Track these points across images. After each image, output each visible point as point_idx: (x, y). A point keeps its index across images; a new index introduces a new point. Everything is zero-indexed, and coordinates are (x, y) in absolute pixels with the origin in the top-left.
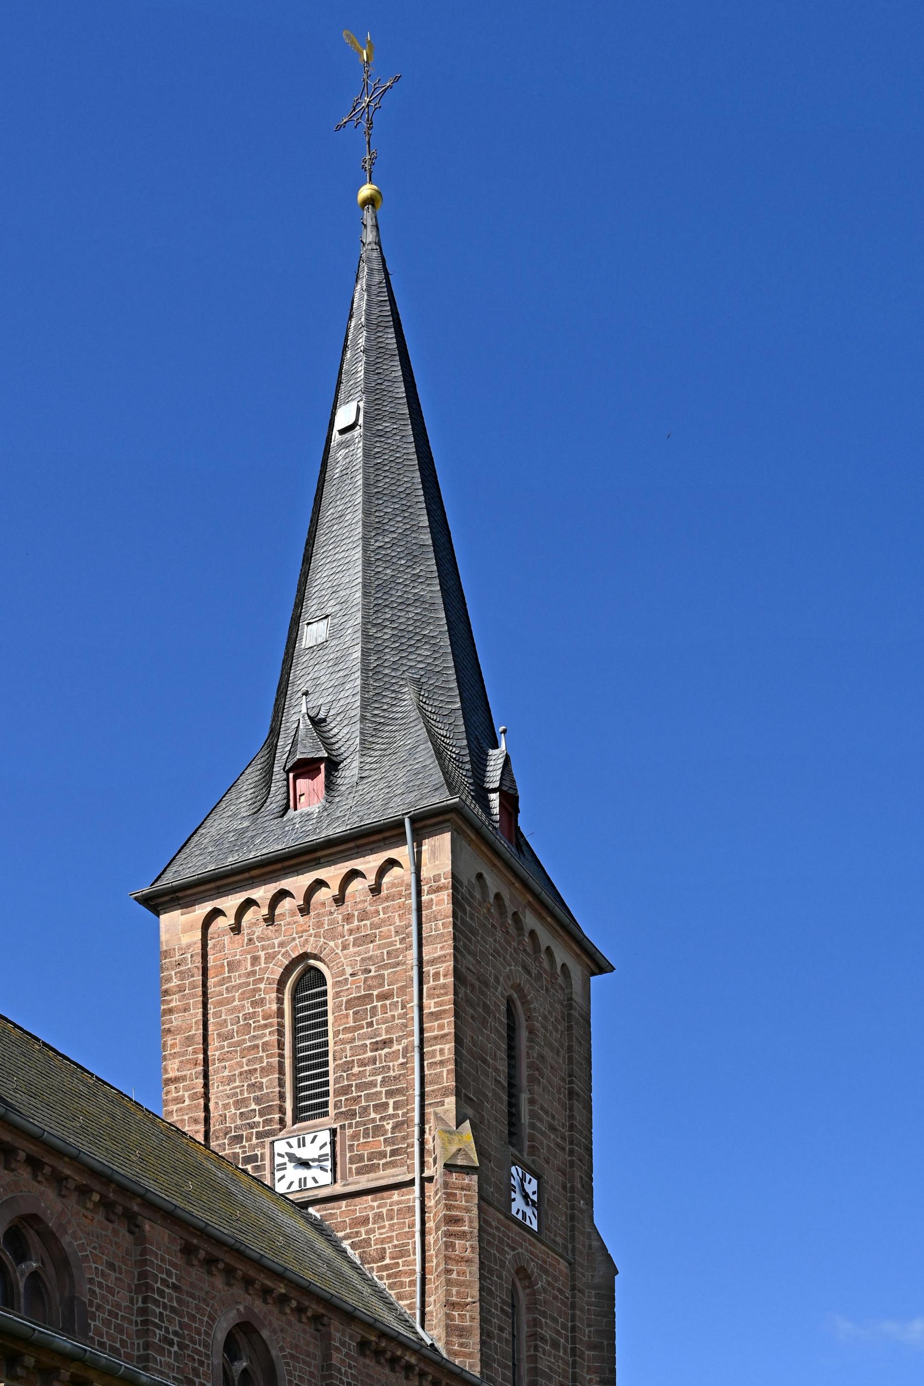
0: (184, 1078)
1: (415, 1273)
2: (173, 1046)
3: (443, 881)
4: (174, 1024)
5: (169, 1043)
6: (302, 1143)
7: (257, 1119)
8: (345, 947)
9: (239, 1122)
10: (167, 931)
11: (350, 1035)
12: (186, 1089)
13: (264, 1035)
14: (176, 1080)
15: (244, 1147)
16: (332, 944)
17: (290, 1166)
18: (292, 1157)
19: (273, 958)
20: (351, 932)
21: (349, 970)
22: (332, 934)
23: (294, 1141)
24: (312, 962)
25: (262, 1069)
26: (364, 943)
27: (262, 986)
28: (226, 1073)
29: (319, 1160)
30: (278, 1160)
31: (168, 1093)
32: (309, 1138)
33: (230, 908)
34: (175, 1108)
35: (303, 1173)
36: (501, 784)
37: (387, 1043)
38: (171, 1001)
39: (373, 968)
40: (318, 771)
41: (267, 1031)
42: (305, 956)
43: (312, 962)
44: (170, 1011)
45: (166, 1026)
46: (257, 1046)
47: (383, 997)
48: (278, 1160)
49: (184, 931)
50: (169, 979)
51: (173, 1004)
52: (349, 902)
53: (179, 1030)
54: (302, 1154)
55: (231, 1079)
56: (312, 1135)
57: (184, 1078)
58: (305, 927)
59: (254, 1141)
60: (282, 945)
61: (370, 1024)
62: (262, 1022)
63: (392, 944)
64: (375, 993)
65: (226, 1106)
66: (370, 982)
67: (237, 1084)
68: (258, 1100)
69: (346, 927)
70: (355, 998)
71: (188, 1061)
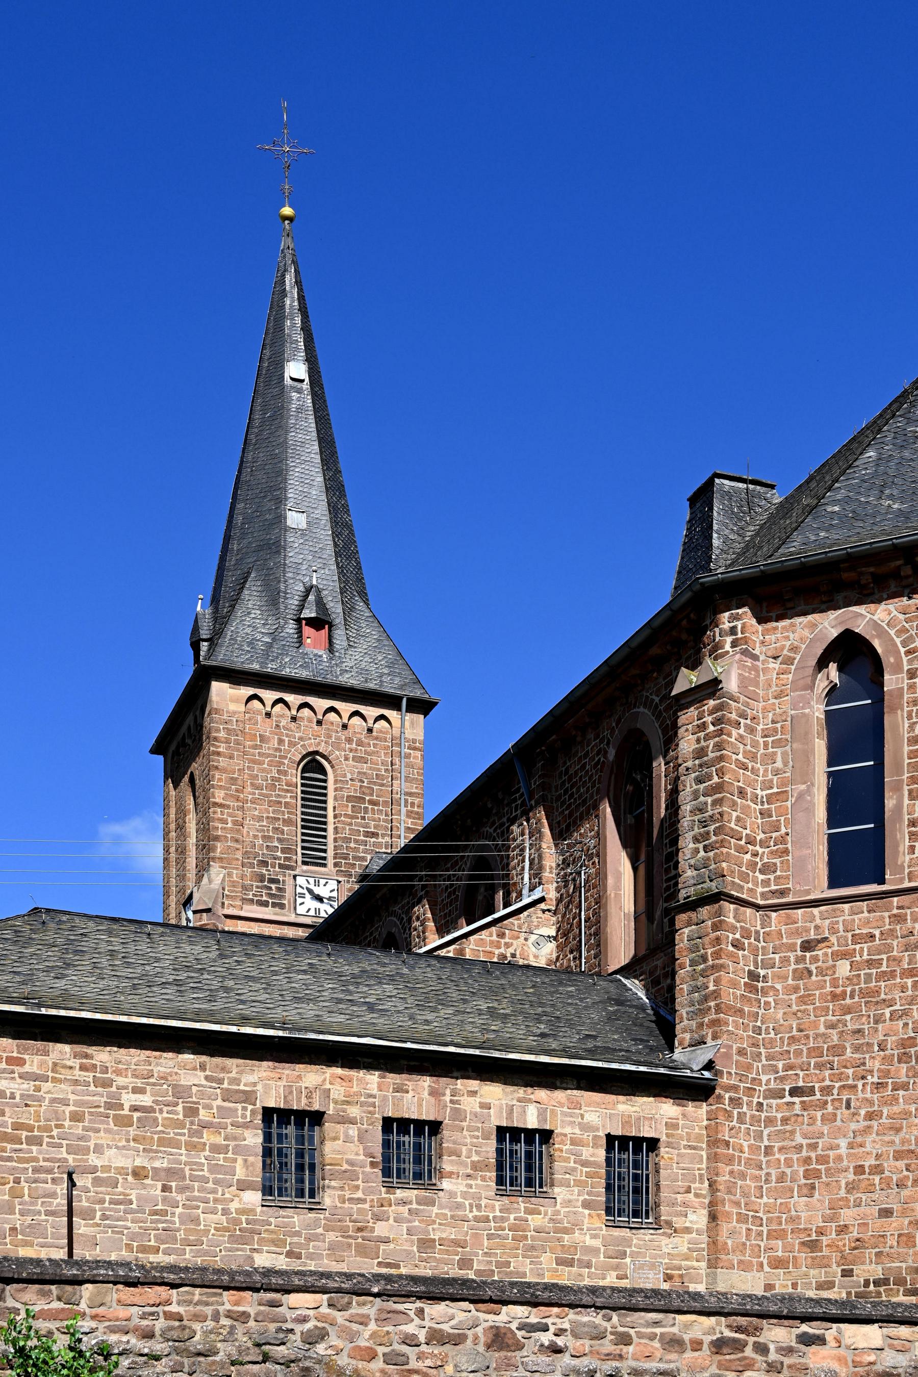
0: (228, 807)
1: (902, 643)
2: (220, 780)
3: (418, 744)
4: (221, 764)
5: (217, 777)
6: (317, 883)
7: (279, 854)
8: (346, 759)
9: (265, 852)
10: (218, 695)
11: (349, 820)
12: (229, 815)
13: (286, 797)
14: (221, 806)
15: (269, 871)
16: (337, 753)
17: (308, 896)
18: (310, 891)
19: (295, 746)
20: (351, 750)
21: (349, 776)
22: (337, 746)
23: (311, 880)
24: (318, 758)
25: (284, 820)
26: (360, 762)
27: (286, 762)
28: (256, 813)
29: (330, 899)
30: (299, 890)
31: (215, 813)
32: (322, 882)
33: (268, 699)
34: (220, 826)
35: (317, 904)
36: (672, 922)
37: (374, 835)
38: (220, 746)
39: (366, 781)
40: (324, 628)
41: (289, 795)
42: (317, 753)
43: (318, 758)
44: (218, 754)
45: (215, 764)
46: (280, 803)
47: (372, 802)
48: (299, 890)
49: (232, 701)
50: (218, 730)
51: (221, 750)
52: (350, 730)
53: (224, 770)
54: (317, 890)
55: (260, 819)
56: (325, 881)
57: (228, 807)
58: (319, 734)
59: (277, 869)
60: (301, 739)
61: (363, 818)
62: (285, 787)
63: (379, 770)
64: (367, 798)
65: (255, 837)
66: (363, 789)
67: (264, 823)
68: (279, 840)
69: (348, 746)
70: (354, 796)
71: (232, 796)
